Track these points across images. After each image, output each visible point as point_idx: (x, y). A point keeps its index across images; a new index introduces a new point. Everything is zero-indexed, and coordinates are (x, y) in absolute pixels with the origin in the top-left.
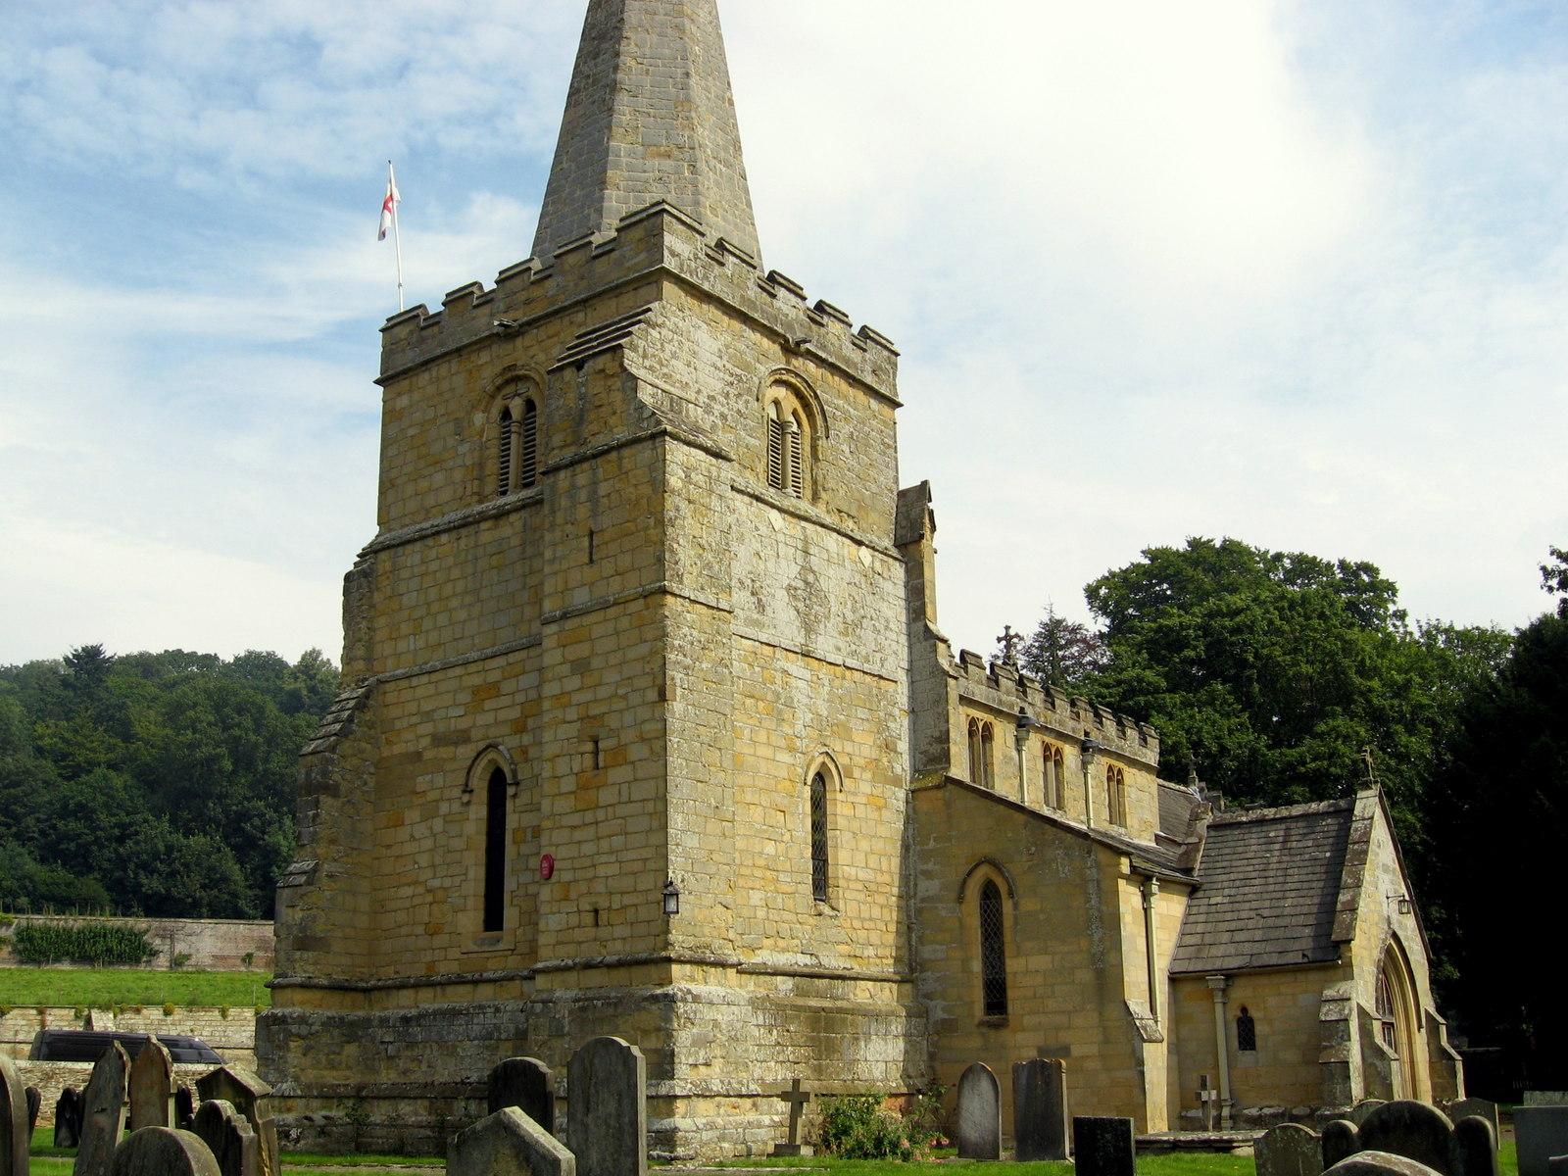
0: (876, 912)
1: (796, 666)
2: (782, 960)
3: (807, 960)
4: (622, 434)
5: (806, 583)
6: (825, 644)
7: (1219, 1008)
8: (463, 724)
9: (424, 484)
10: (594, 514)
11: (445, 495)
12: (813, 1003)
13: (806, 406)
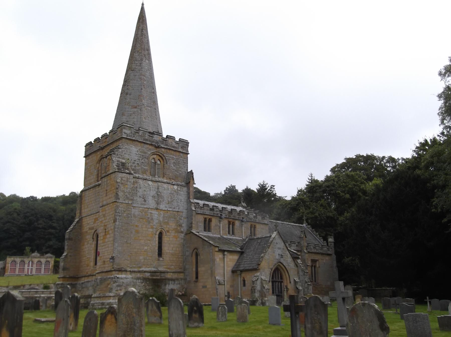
0: (175, 259)
1: (154, 212)
2: (147, 269)
3: (155, 269)
4: (111, 172)
5: (158, 195)
6: (162, 207)
7: (239, 278)
8: (93, 226)
9: (90, 178)
10: (107, 187)
11: (93, 181)
12: (154, 278)
13: (162, 158)
